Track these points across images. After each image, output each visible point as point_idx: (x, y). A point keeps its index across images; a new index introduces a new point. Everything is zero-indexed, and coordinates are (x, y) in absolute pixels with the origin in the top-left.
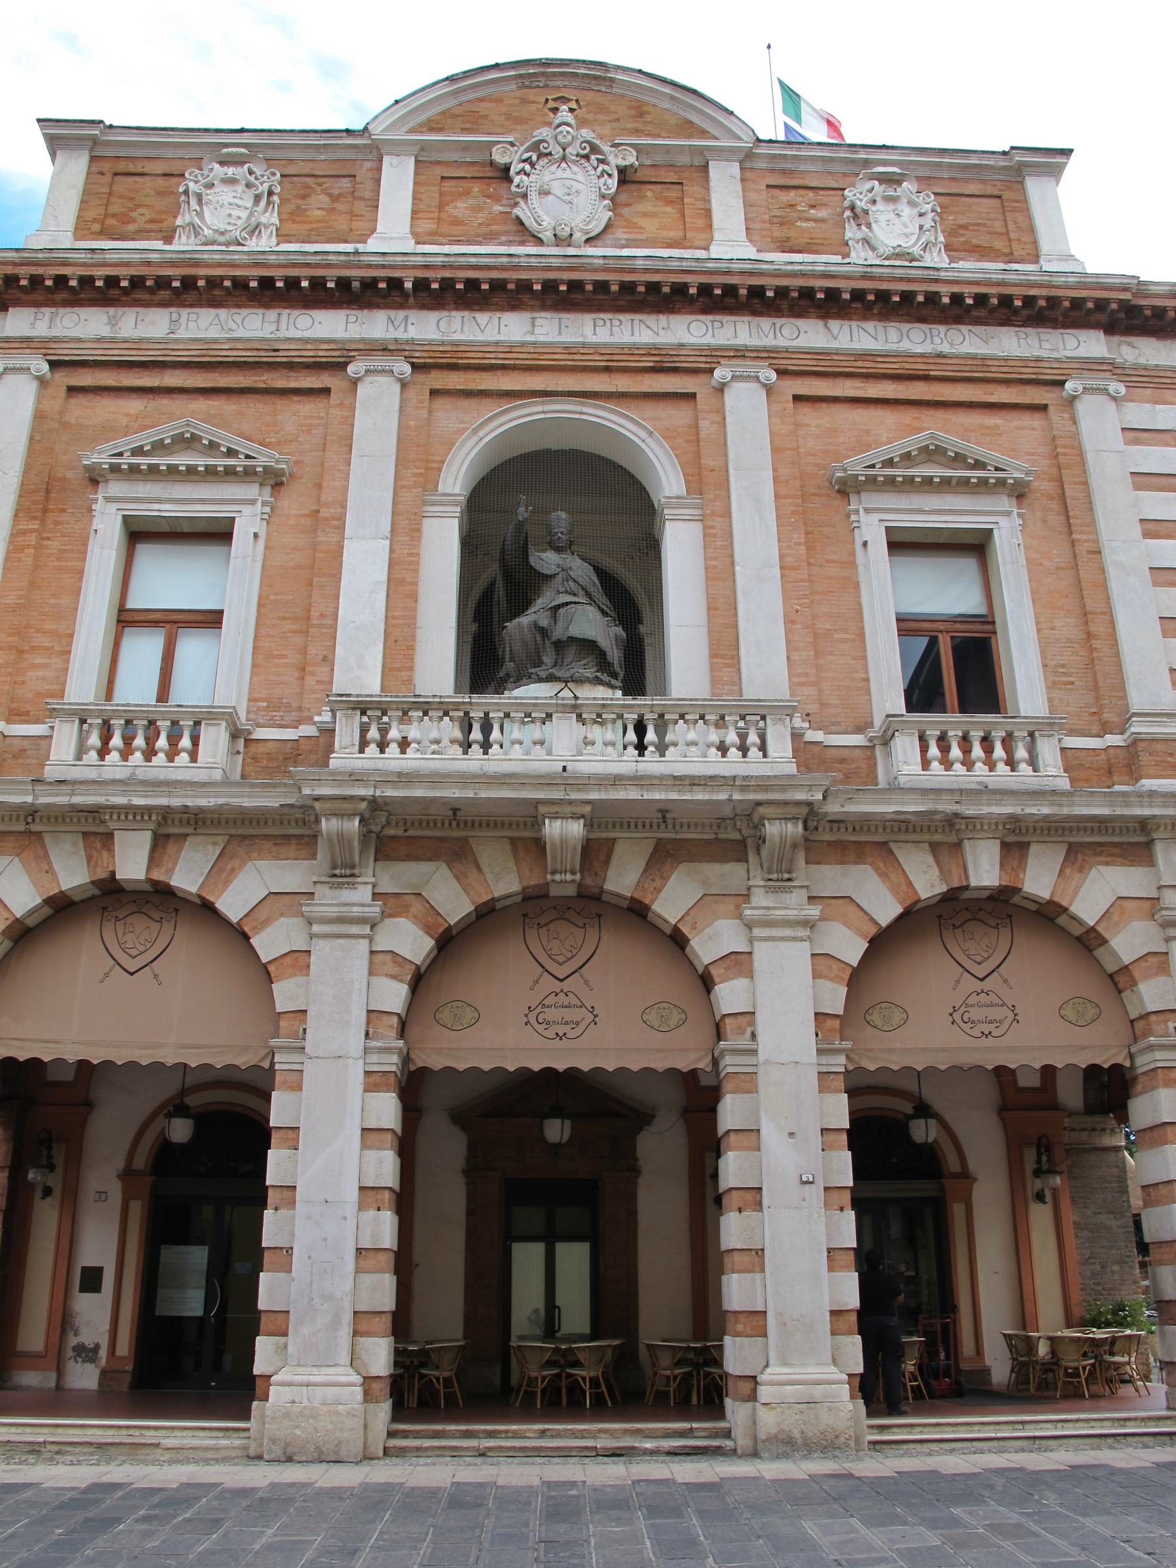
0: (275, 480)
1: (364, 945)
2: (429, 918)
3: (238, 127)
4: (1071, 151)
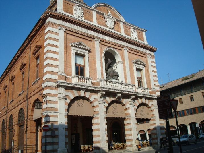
0: (89, 51)
1: (103, 105)
2: (107, 102)
4: (4, 119)
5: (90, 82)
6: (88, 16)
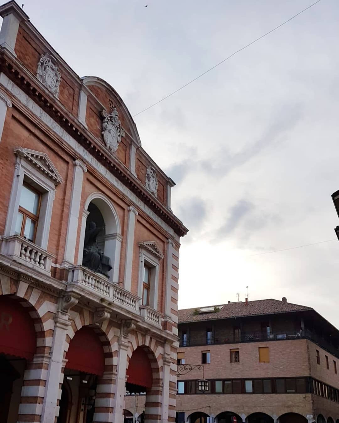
3: (57, 52)
5: (50, 263)
6: (69, 98)
